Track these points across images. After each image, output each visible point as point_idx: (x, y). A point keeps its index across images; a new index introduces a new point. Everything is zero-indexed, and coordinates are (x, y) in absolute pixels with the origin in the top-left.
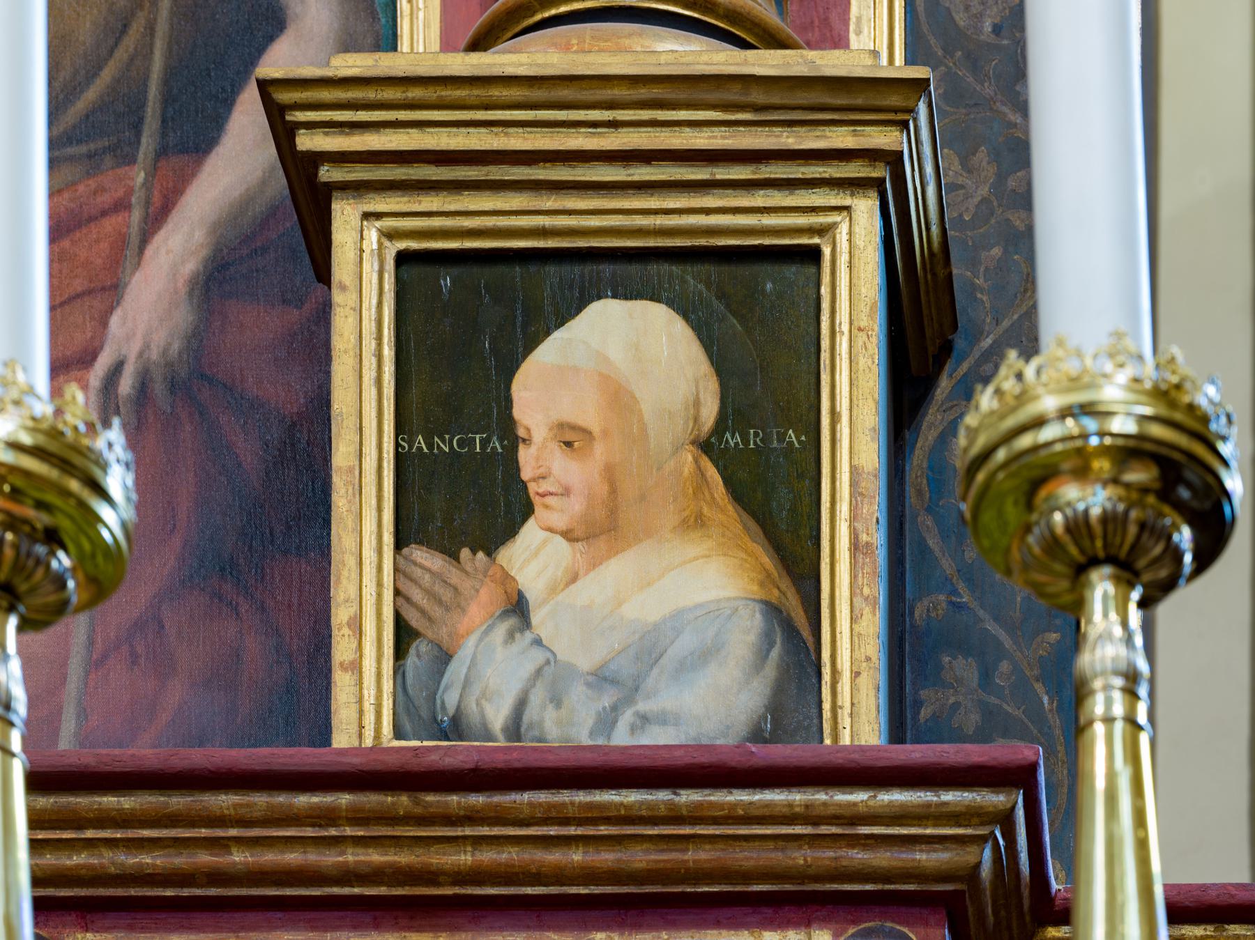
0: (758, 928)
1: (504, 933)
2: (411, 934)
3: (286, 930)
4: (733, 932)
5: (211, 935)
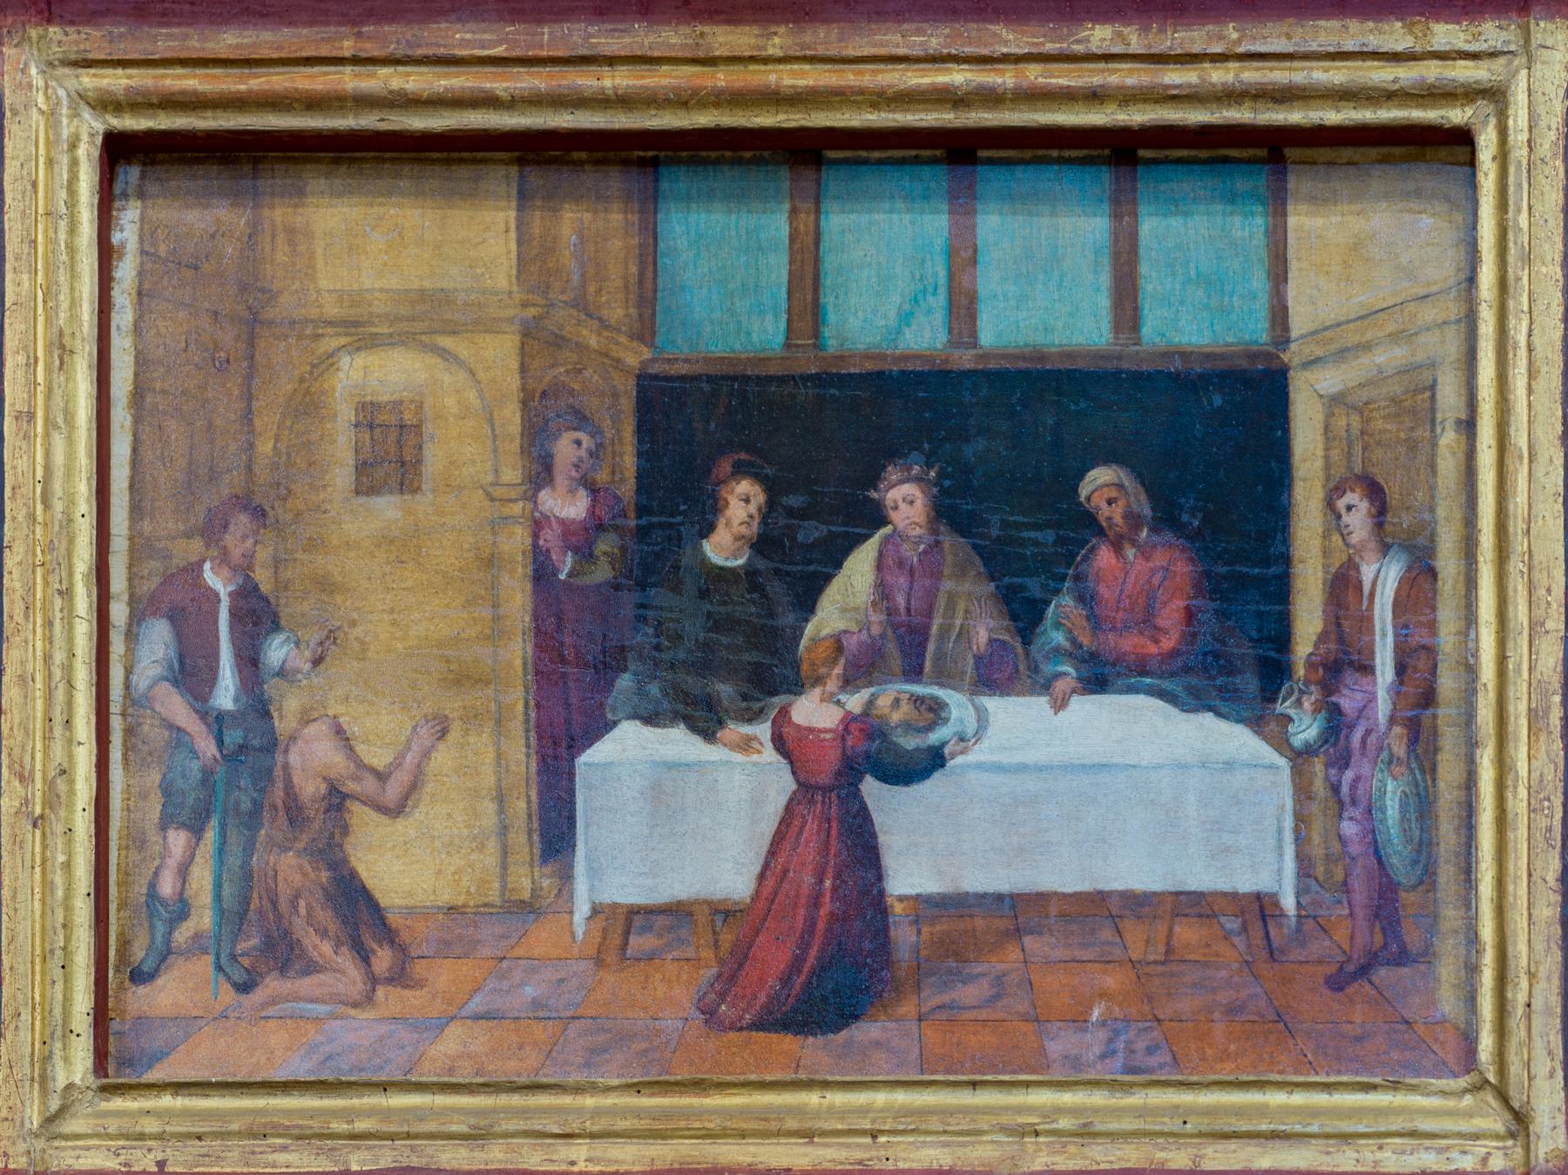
0: (1422, 14)
1: (906, 26)
2: (715, 29)
3: (459, 20)
4: (1371, 24)
5: (305, 31)
